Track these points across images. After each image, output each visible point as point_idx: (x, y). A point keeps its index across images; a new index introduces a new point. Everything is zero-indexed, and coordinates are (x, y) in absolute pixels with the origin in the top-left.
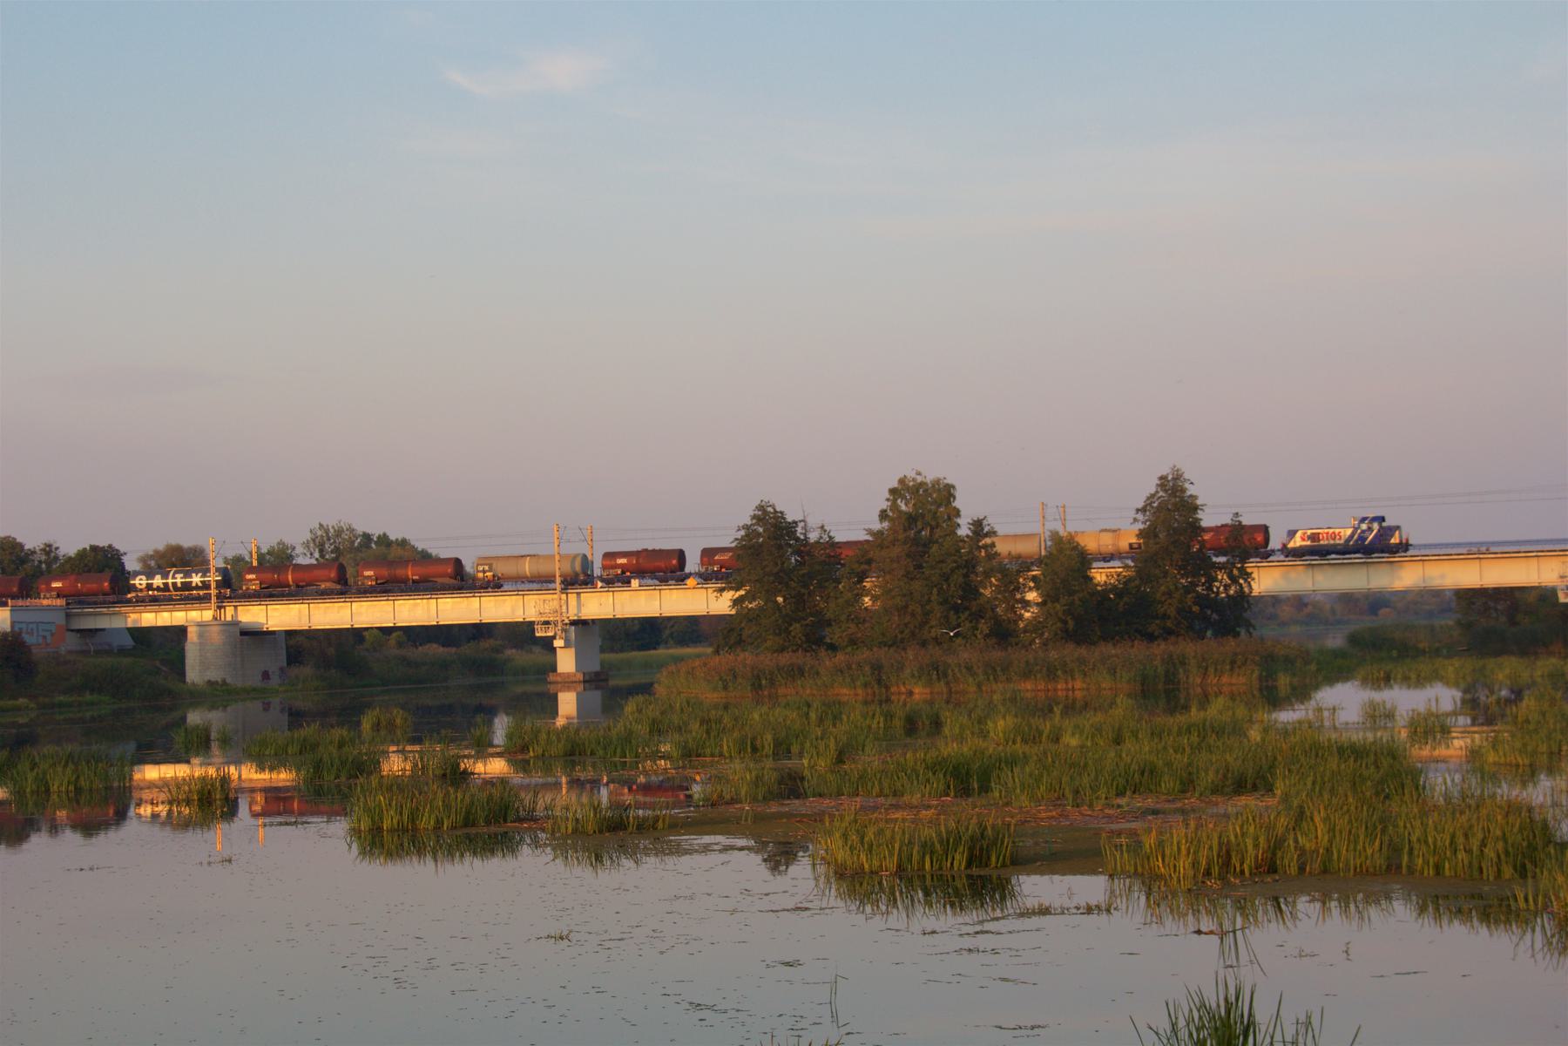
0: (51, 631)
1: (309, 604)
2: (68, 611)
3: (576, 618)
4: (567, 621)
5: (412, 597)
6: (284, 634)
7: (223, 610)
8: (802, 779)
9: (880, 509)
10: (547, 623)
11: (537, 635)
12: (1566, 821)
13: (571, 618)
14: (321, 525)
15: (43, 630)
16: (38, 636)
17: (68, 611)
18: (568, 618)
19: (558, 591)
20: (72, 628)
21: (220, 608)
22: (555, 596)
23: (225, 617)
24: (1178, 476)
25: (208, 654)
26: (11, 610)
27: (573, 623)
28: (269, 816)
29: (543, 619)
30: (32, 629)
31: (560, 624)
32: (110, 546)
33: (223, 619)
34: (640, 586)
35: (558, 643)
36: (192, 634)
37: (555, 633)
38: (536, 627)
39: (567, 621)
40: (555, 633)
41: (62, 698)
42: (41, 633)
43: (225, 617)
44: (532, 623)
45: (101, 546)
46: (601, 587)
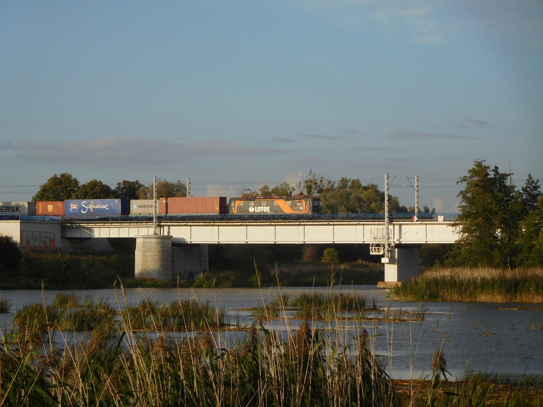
0: (50, 238)
1: (169, 226)
2: (63, 224)
3: (398, 242)
4: (393, 244)
5: (287, 223)
6: (107, 242)
7: (162, 229)
8: (325, 361)
9: (133, 181)
10: (378, 245)
11: (371, 253)
12: (513, 402)
13: (395, 243)
14: (496, 168)
15: (45, 237)
16: (40, 241)
17: (63, 224)
18: (394, 242)
19: (386, 223)
20: (66, 237)
21: (160, 226)
22: (384, 227)
23: (163, 234)
24: (479, 165)
25: (148, 258)
26: (21, 223)
27: (399, 246)
28: (351, 394)
29: (376, 243)
30: (36, 236)
31: (387, 247)
32: (358, 180)
33: (162, 234)
34: (444, 221)
35: (385, 260)
36: (139, 242)
37: (384, 253)
38: (370, 248)
39: (393, 244)
40: (384, 253)
41: (308, 292)
42: (42, 239)
43: (163, 234)
44: (368, 245)
45: (131, 181)
46: (416, 221)
